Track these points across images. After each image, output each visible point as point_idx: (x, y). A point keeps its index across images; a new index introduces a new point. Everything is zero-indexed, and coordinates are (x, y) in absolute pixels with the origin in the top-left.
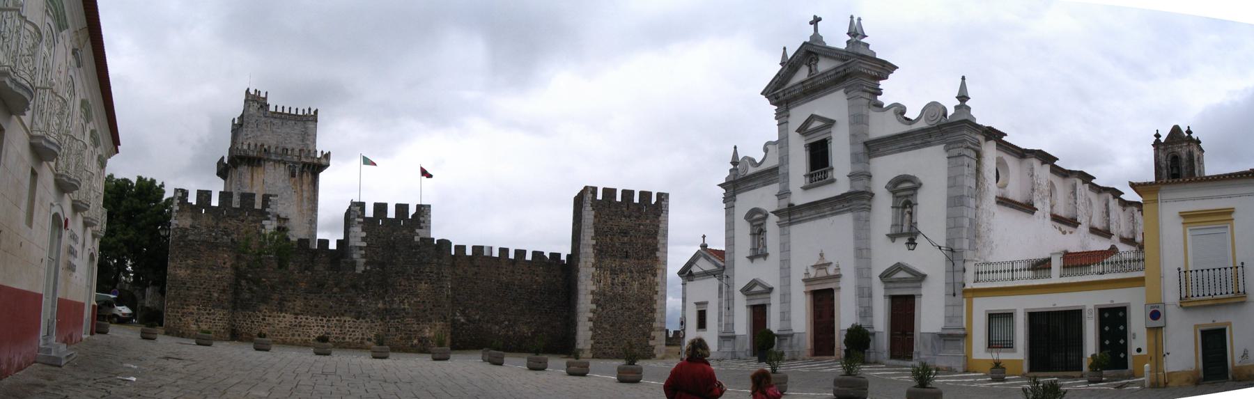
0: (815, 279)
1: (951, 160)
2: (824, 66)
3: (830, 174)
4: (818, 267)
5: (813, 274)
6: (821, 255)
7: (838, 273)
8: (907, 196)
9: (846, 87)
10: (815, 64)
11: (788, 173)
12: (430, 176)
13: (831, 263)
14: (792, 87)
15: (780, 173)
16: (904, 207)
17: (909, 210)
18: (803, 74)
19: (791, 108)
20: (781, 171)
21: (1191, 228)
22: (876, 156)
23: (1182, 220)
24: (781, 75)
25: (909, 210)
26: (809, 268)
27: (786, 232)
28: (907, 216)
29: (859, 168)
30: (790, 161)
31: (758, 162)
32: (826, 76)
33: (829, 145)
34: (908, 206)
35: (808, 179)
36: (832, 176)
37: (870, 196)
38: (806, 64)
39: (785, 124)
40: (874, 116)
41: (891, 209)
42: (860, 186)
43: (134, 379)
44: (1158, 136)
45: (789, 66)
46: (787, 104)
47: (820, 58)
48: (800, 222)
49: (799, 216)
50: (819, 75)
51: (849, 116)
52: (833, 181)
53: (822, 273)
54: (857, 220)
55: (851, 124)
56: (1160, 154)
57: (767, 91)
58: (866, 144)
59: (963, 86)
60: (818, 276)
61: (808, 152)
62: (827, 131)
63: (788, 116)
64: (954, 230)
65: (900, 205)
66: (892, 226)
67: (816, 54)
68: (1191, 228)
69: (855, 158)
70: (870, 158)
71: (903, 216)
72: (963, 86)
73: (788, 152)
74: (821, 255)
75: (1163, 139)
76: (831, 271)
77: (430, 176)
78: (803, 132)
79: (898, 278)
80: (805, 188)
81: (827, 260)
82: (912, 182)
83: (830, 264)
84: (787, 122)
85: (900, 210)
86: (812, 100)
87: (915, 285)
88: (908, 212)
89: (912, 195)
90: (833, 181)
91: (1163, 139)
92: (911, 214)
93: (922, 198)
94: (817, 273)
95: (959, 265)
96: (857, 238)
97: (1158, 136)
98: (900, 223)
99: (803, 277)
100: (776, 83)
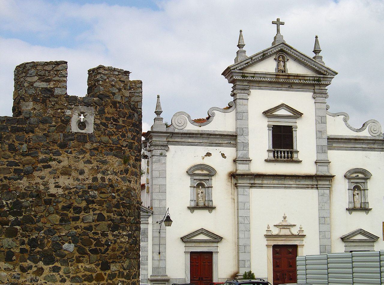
0: (277, 236)
3: (295, 155)
5: (275, 231)
6: (285, 218)
12: (225, 157)
13: (294, 225)
21: (154, 283)
23: (266, 239)
29: (322, 157)
31: (208, 116)
33: (294, 132)
35: (271, 154)
42: (323, 171)
43: (32, 249)
45: (264, 55)
50: (286, 75)
52: (299, 162)
54: (321, 196)
59: (158, 106)
60: (281, 234)
61: (271, 132)
62: (294, 120)
68: (154, 283)
72: (158, 106)
74: (285, 218)
76: (295, 231)
77: (225, 157)
78: (269, 114)
79: (195, 240)
81: (290, 221)
82: (207, 170)
86: (278, 90)
87: (369, 244)
90: (299, 162)
93: (370, 184)
96: (320, 209)
99: (265, 233)
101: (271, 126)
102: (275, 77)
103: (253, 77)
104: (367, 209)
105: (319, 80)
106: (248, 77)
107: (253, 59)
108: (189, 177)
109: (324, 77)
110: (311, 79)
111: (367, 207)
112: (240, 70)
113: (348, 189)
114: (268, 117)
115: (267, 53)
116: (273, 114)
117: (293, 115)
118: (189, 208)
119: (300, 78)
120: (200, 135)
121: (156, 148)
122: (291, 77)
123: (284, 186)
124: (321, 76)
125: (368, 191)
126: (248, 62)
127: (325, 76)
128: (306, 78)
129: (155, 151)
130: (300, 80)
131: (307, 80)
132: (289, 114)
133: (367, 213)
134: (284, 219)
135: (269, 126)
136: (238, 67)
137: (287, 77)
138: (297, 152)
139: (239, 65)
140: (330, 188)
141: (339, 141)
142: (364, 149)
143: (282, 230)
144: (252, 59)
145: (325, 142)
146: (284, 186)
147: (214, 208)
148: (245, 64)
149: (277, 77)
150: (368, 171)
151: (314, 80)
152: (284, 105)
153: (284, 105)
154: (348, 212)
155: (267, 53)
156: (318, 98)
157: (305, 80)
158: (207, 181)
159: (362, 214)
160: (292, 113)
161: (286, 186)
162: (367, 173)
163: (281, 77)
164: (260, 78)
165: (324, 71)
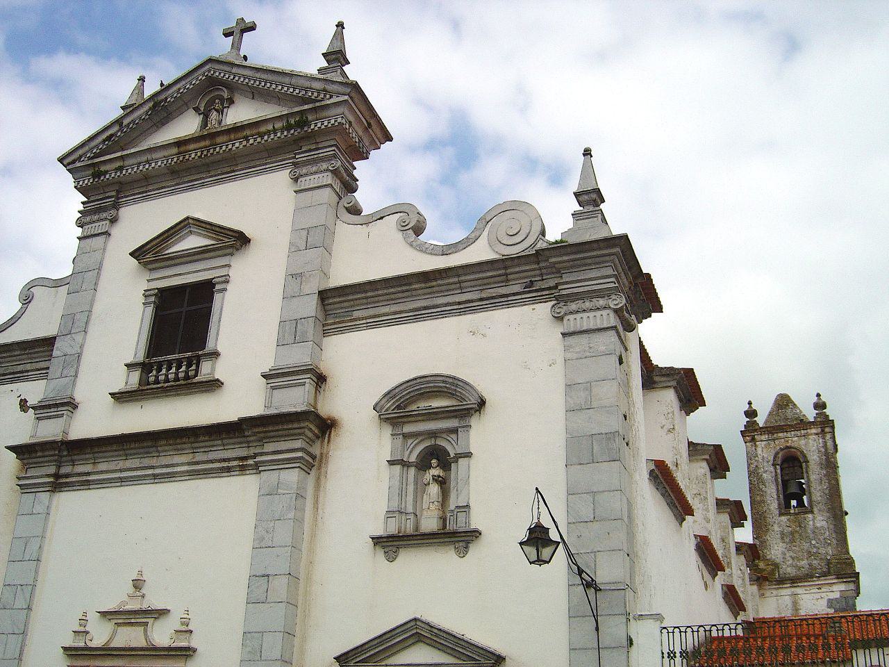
1: (571, 340)
2: (241, 112)
4: (119, 617)
5: (100, 635)
6: (138, 584)
7: (184, 644)
8: (433, 434)
9: (295, 164)
10: (220, 112)
11: (79, 356)
14: (150, 150)
15: (55, 353)
16: (423, 464)
17: (436, 472)
18: (187, 125)
19: (127, 204)
20: (60, 348)
22: (341, 331)
24: (125, 122)
25: (436, 472)
26: (93, 617)
27: (38, 509)
28: (434, 489)
30: (91, 329)
32: (270, 127)
33: (217, 297)
34: (434, 462)
35: (135, 377)
36: (212, 372)
37: (327, 427)
38: (197, 109)
39: (101, 239)
40: (347, 234)
41: (386, 471)
42: (294, 399)
44: (751, 413)
45: (154, 106)
46: (118, 192)
47: (237, 98)
48: (86, 485)
49: (88, 468)
51: (294, 231)
52: (214, 385)
53: (130, 637)
55: (294, 249)
56: (759, 451)
57: (80, 152)
58: (324, 295)
60: (118, 642)
61: (150, 310)
63: (114, 221)
64: (596, 525)
65: (413, 458)
66: (390, 514)
67: (231, 87)
69: (290, 332)
70: (326, 333)
71: (421, 488)
73: (92, 306)
74: (138, 584)
75: (761, 420)
76: (162, 635)
78: (149, 257)
80: (121, 397)
81: (154, 600)
82: (451, 395)
83: (161, 613)
84: (107, 234)
85: (412, 471)
86: (192, 188)
88: (436, 479)
89: (455, 431)
90: (214, 385)
91: (761, 420)
92: (442, 482)
94: (114, 633)
95: (613, 629)
97: (751, 413)
98: (410, 509)
100: (109, 138)
101: (152, 292)
102: (175, 150)
103: (120, 168)
104: (454, 534)
105: (303, 123)
106: (106, 172)
107: (125, 122)
108: (388, 430)
109: (315, 110)
110: (278, 125)
111: (461, 526)
112: (90, 158)
113: (391, 463)
114: (150, 270)
115: (166, 98)
116: (167, 252)
117: (213, 242)
118: (377, 541)
119: (248, 132)
120: (21, 350)
121: (573, 306)
122: (219, 140)
123: (150, 472)
124: (306, 107)
125: (473, 461)
126: (112, 135)
127: (318, 104)
128: (263, 129)
129: (571, 317)
130: (246, 138)
131: (268, 133)
132: (203, 245)
133: (463, 551)
134: (135, 587)
135: (147, 293)
136: (85, 154)
137: (207, 143)
138: (215, 354)
139: (87, 148)
140: (312, 464)
141: (369, 294)
142: (464, 308)
143: (120, 629)
144: (121, 125)
145: (310, 306)
146: (150, 472)
147: (475, 534)
148: (104, 141)
149: (182, 149)
150: (461, 381)
151: (288, 128)
152: (190, 221)
153: (190, 221)
154: (380, 554)
155: (166, 98)
156: (308, 178)
157: (261, 135)
158: (454, 436)
159: (442, 560)
160: (213, 239)
161: (157, 471)
162: (462, 388)
163: (192, 146)
164: (262, 137)
165: (319, 92)
